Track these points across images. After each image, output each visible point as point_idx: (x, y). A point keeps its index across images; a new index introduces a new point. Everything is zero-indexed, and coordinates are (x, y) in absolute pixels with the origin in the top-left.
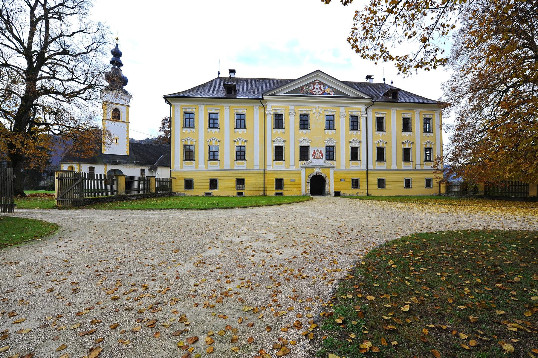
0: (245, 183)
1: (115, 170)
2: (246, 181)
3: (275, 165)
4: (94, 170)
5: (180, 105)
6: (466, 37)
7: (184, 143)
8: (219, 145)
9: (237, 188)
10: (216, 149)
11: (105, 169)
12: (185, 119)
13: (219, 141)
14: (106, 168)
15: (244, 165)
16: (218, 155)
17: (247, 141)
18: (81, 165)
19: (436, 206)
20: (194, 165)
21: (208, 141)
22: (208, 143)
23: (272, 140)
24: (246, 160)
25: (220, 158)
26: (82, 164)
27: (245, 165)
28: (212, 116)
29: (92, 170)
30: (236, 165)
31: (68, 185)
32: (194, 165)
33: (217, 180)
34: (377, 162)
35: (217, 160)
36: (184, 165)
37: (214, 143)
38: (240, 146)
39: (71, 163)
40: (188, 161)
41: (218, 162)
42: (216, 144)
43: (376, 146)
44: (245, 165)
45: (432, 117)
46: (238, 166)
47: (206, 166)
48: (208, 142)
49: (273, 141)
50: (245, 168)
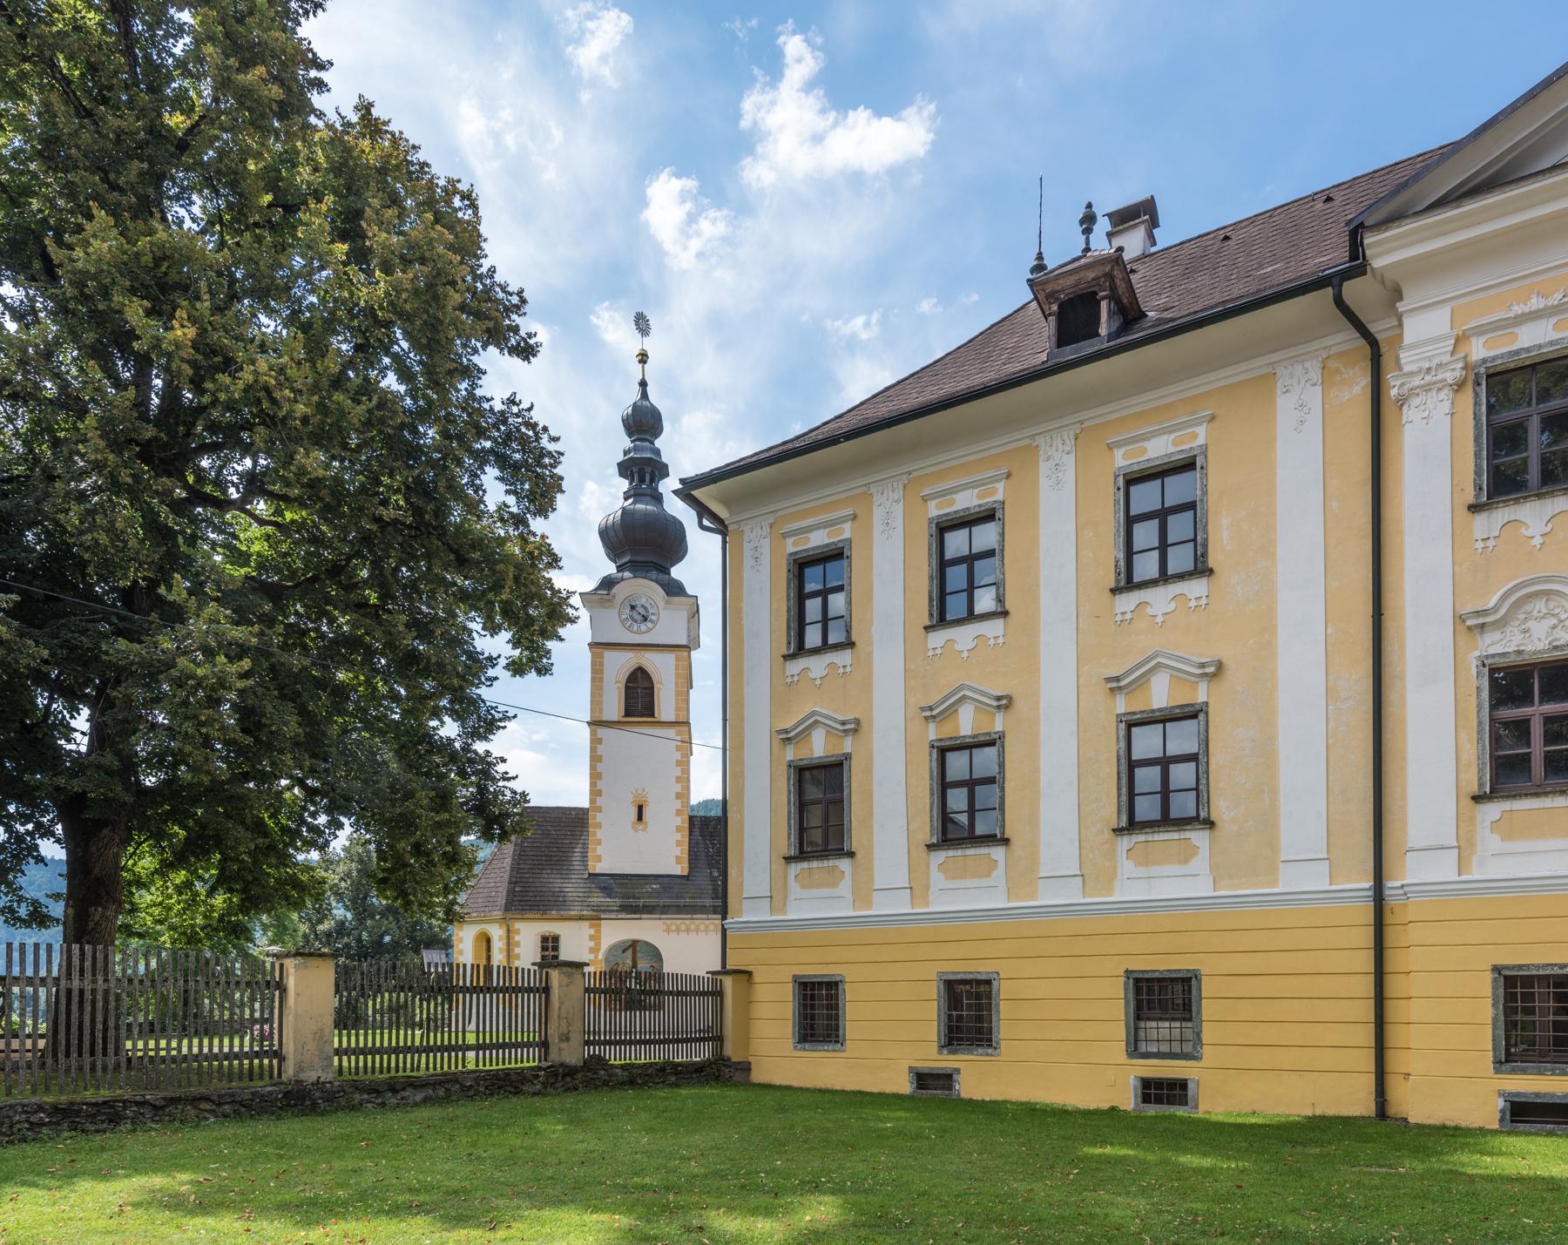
0: (1208, 1010)
1: (634, 945)
2: (1208, 987)
3: (1490, 842)
4: (556, 948)
5: (771, 519)
6: (341, 248)
7: (790, 754)
8: (1002, 736)
9: (1135, 1049)
10: (985, 760)
11: (596, 938)
12: (1130, 521)
13: (1005, 703)
14: (599, 932)
15: (1190, 868)
16: (1199, 790)
17: (1216, 672)
18: (518, 925)
19: (395, 1221)
20: (845, 887)
21: (1115, 685)
22: (932, 733)
23: (1459, 619)
24: (851, 854)
25: (1014, 826)
26: (872, 879)
27: (1200, 863)
28: (1146, 497)
29: (550, 944)
30: (1126, 867)
31: (457, 1032)
32: (845, 887)
33: (988, 982)
34: (940, 856)
35: (991, 839)
36: (937, 879)
37: (966, 724)
38: (1164, 721)
39: (482, 922)
40: (815, 864)
41: (998, 853)
42: (1183, 698)
43: (932, 736)
44: (1200, 863)
45: (847, 531)
46: (1142, 871)
47: (918, 889)
48: (932, 726)
49: (1471, 624)
50: (998, 901)
